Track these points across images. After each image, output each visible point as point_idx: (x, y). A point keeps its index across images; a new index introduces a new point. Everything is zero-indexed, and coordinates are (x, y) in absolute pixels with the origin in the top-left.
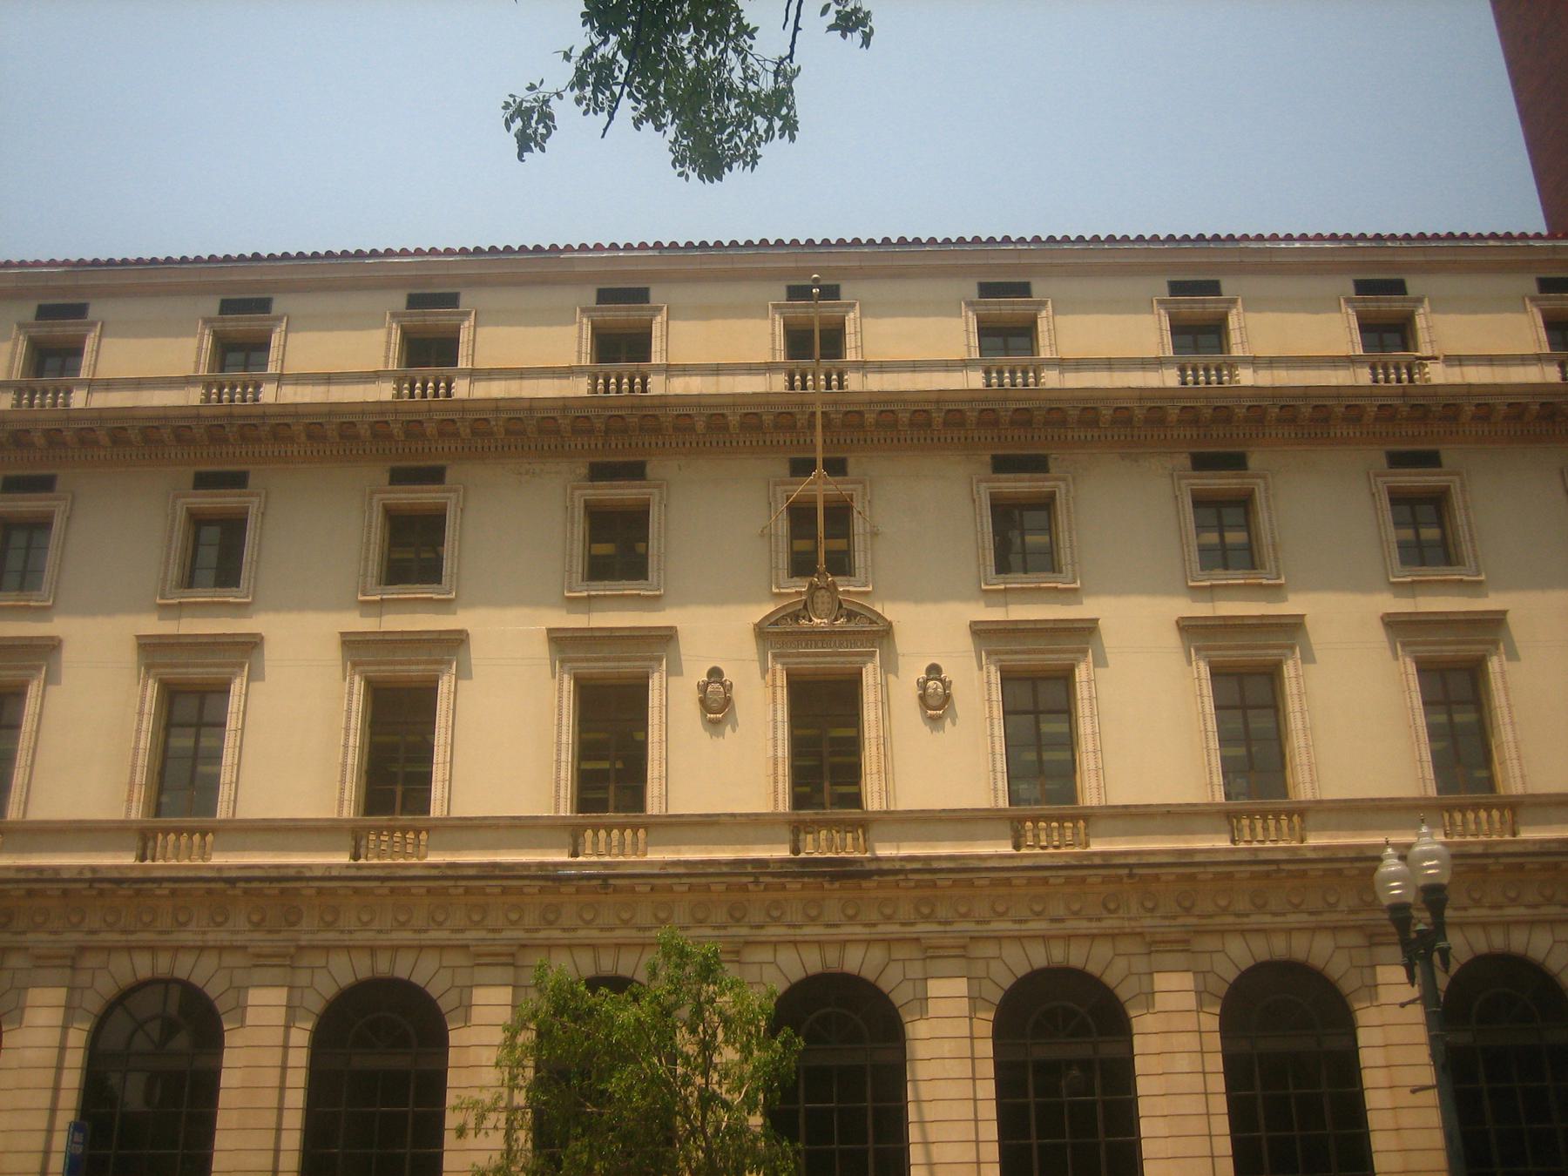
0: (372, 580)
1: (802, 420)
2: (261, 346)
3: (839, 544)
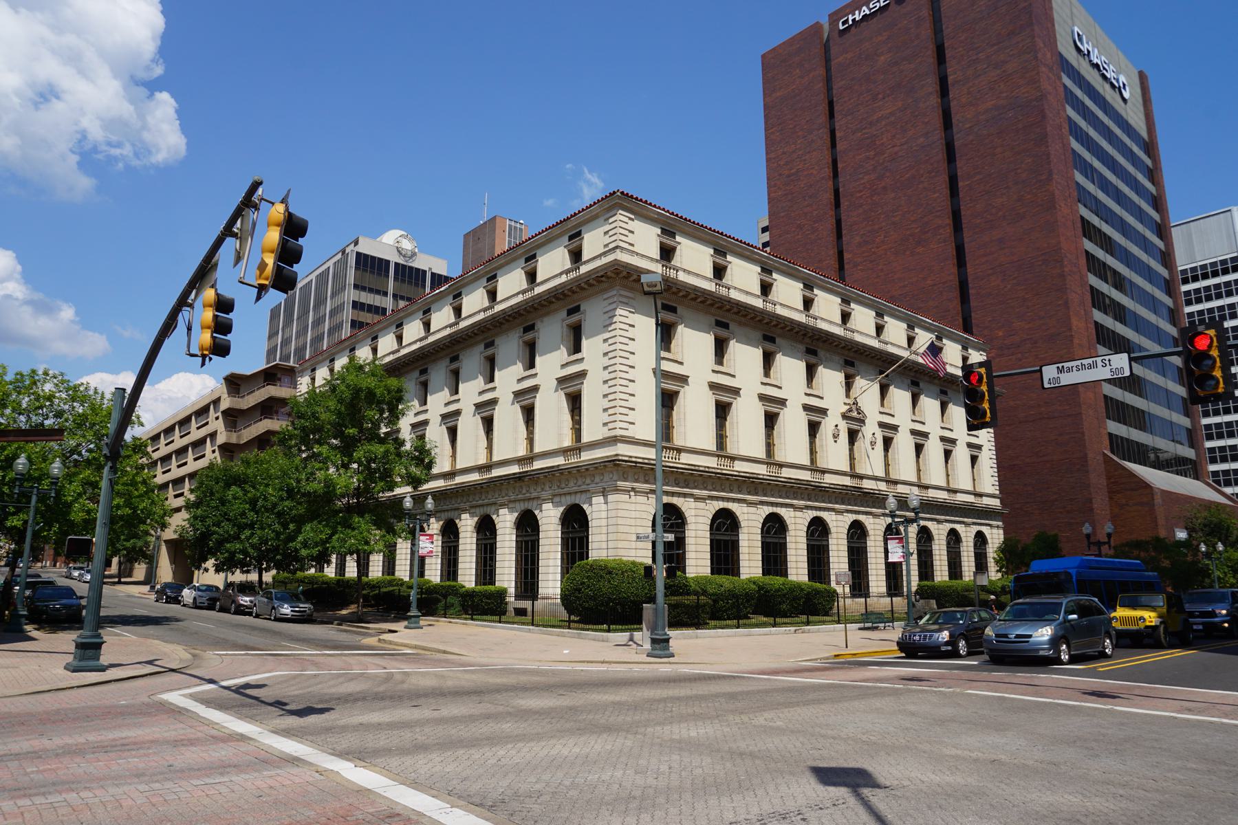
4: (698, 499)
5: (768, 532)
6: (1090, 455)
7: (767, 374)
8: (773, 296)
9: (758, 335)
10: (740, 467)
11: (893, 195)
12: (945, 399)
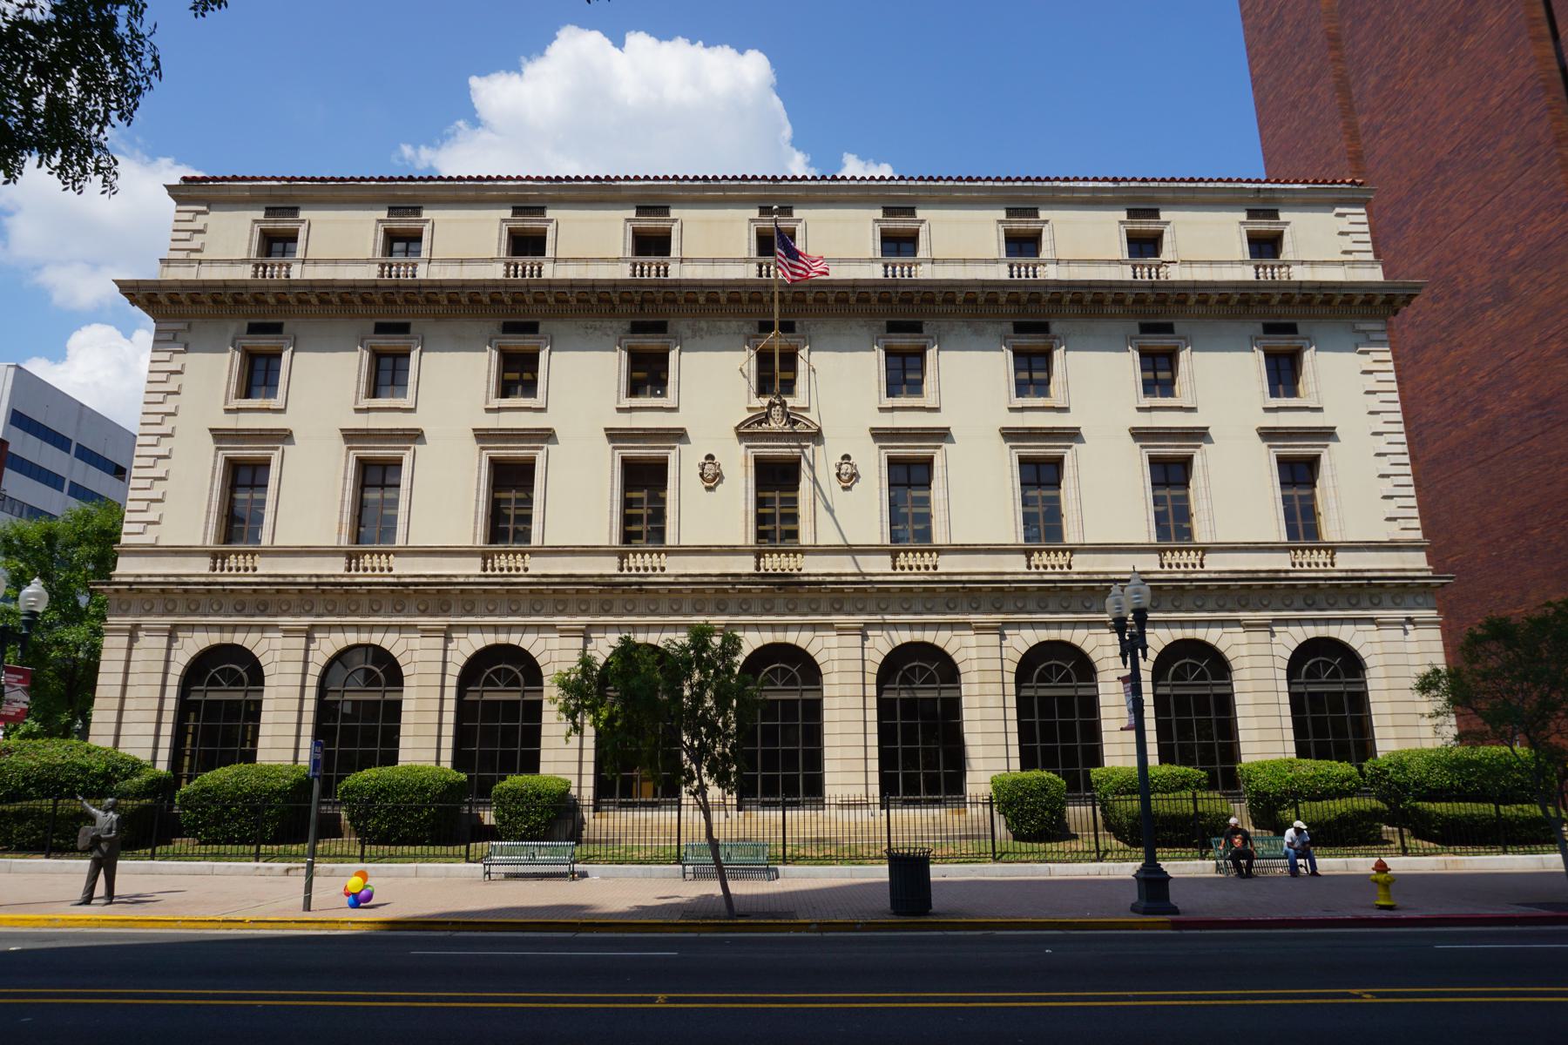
0: (753, 395)
1: (766, 298)
2: (292, 237)
3: (788, 375)
4: (1249, 626)
9: (493, 326)
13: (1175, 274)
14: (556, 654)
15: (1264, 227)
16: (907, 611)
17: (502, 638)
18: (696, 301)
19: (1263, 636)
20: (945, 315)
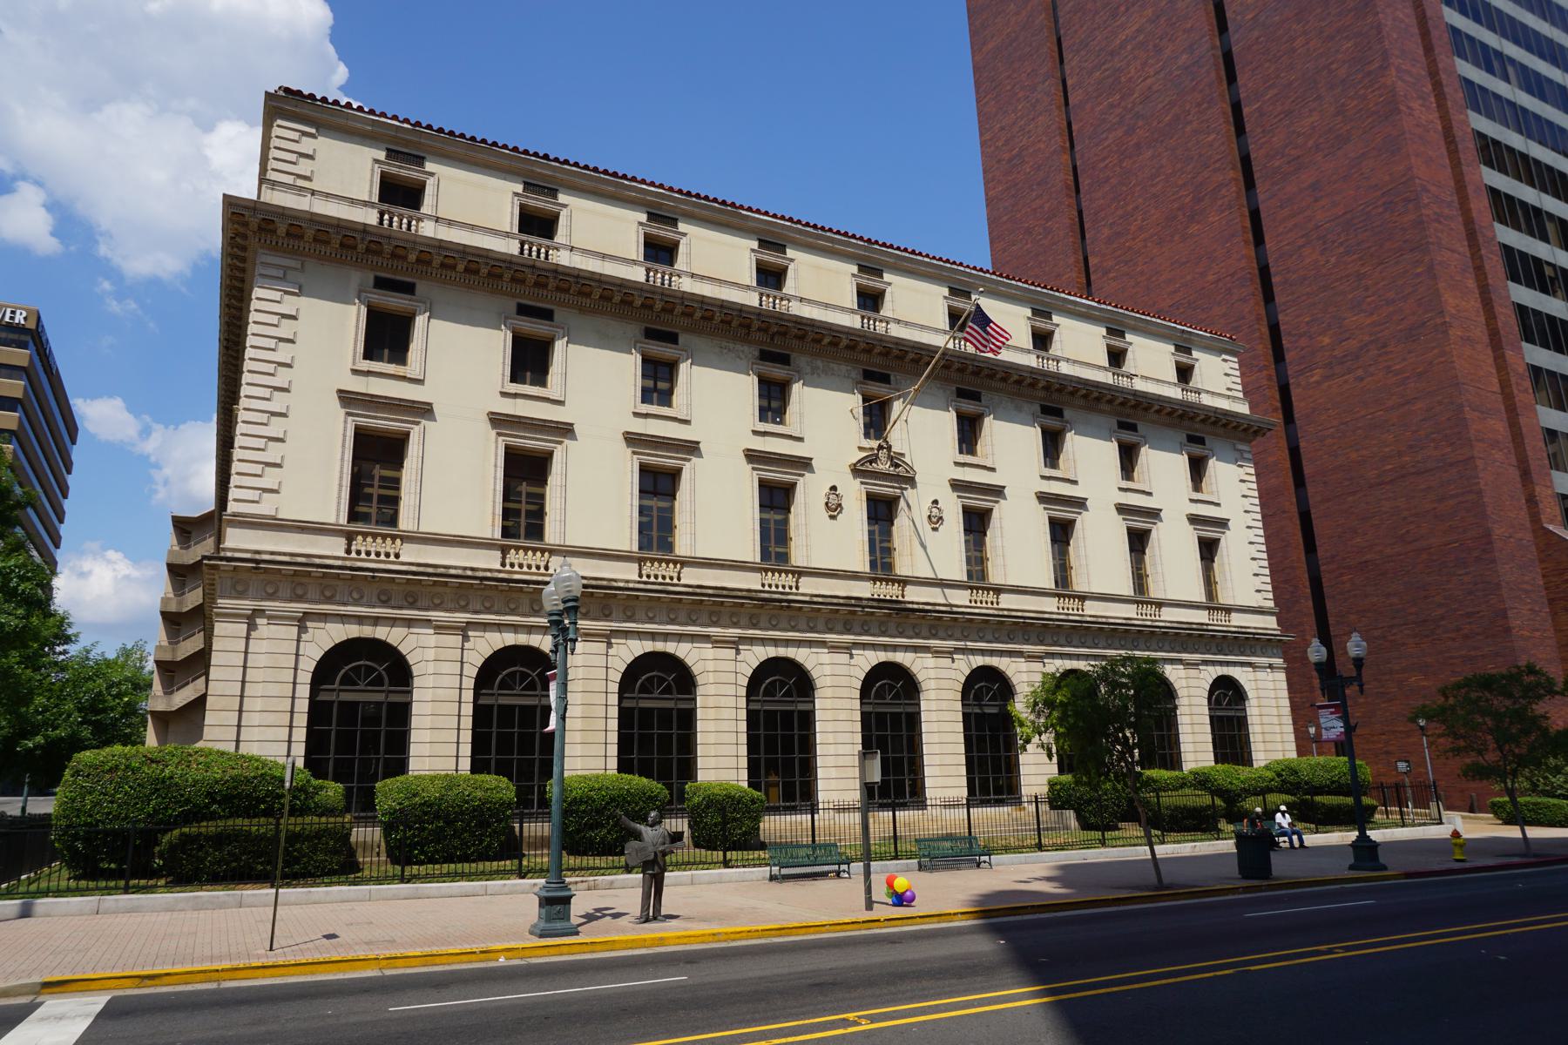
5: (1218, 702)
6: (1498, 531)
7: (1197, 487)
8: (1129, 366)
9: (635, 330)
10: (1170, 615)
11: (1149, 153)
12: (777, 372)
13: (563, 258)
14: (1026, 675)
15: (772, 259)
16: (981, 639)
17: (659, 646)
18: (404, 258)
19: (844, 658)
20: (997, 390)
